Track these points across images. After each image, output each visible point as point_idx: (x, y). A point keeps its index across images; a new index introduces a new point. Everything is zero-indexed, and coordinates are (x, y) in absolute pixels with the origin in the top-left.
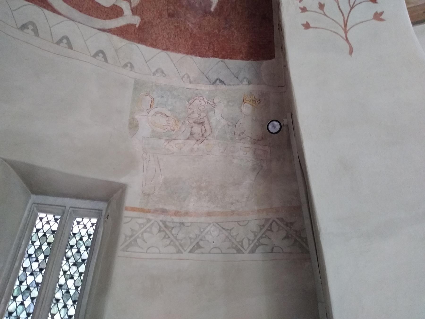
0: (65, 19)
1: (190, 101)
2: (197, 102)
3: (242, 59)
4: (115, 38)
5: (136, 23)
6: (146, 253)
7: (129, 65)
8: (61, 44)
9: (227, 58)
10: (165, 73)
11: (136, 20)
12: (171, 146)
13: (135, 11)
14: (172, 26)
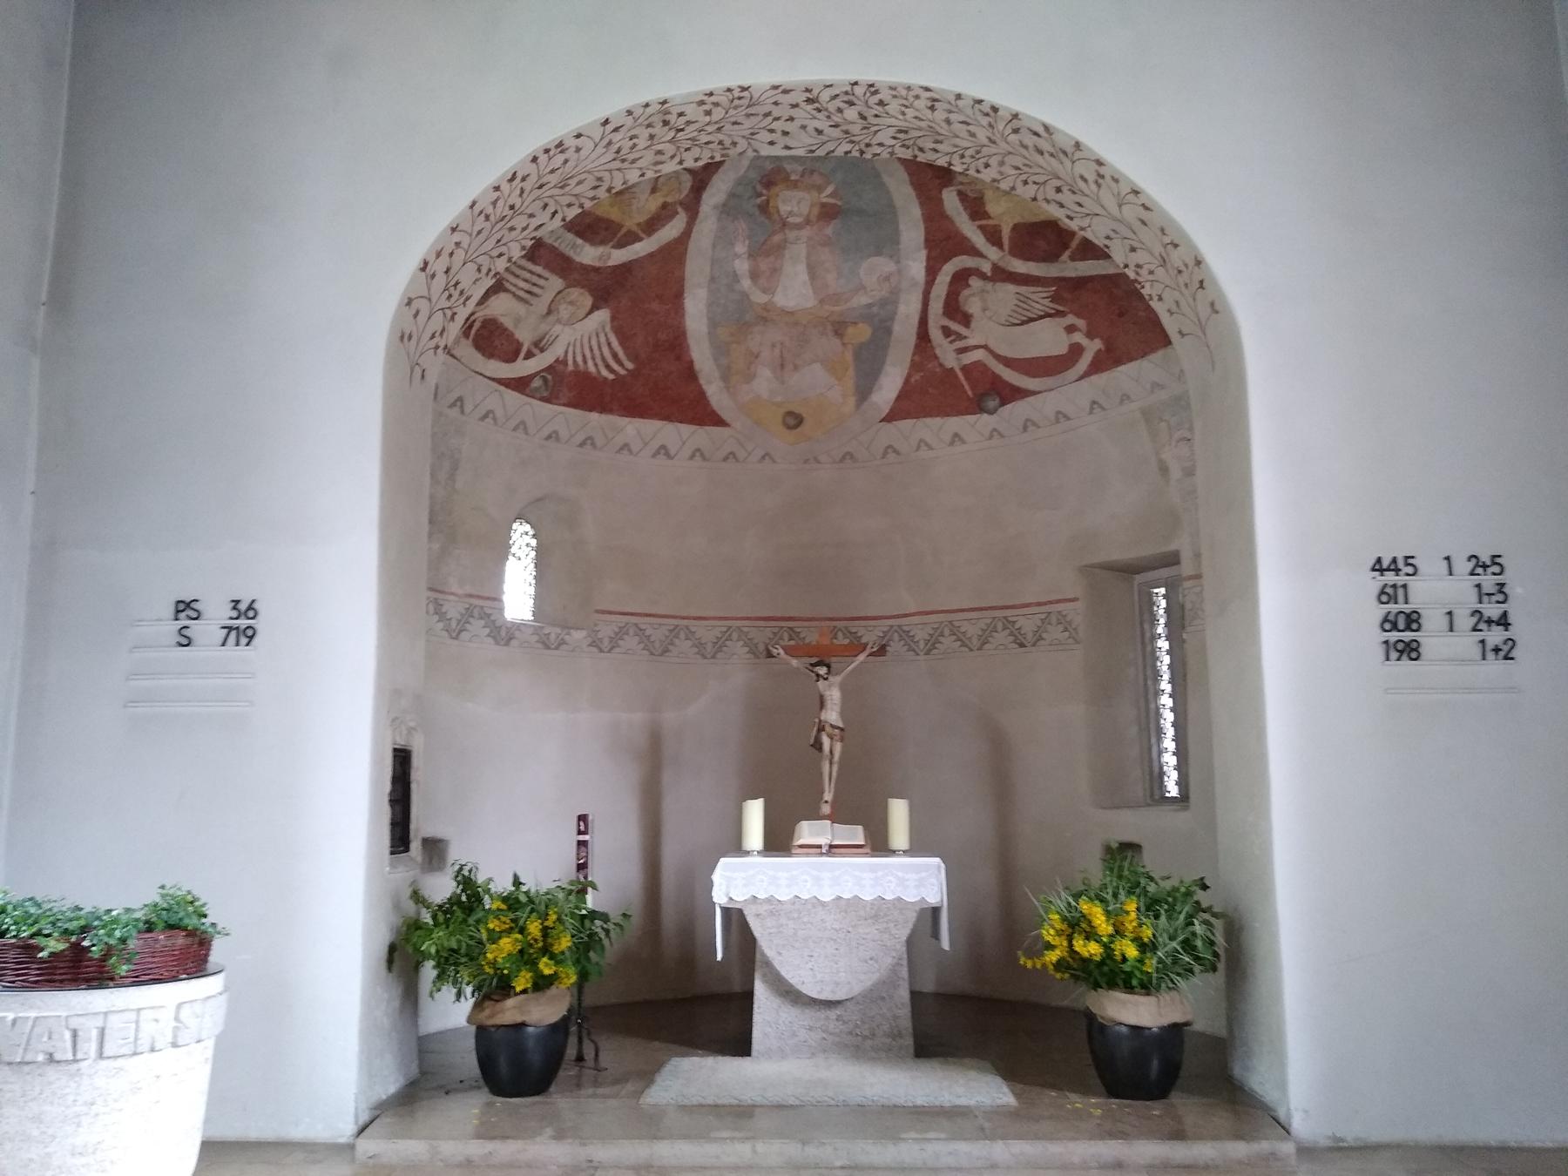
4: (1094, 378)
6: (750, 454)
8: (487, 420)
13: (1090, 335)
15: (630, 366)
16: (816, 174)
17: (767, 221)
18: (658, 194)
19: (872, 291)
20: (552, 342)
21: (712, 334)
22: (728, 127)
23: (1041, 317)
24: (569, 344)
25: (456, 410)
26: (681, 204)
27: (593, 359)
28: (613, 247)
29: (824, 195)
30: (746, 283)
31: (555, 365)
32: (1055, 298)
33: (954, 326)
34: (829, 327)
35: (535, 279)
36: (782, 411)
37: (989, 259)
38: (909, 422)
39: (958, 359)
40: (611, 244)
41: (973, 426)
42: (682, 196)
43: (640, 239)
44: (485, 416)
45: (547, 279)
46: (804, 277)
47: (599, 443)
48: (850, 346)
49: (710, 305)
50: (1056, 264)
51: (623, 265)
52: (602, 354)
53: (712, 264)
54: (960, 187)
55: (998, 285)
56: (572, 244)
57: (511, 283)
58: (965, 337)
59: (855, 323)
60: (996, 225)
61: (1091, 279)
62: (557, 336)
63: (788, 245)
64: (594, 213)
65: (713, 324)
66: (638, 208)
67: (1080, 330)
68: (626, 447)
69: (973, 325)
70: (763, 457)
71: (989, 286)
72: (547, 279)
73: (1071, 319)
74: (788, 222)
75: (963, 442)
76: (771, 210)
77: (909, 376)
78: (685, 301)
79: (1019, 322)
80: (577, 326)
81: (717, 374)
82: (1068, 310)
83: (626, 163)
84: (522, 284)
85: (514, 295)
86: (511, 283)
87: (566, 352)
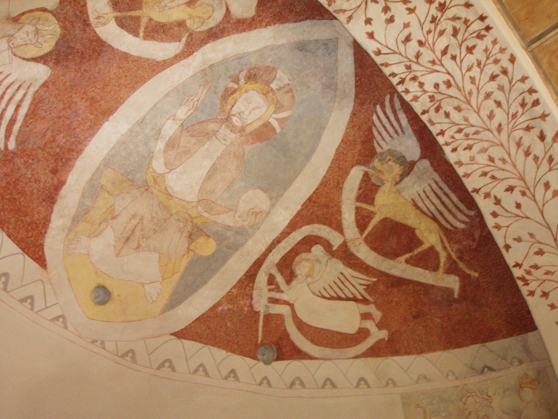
0: (322, 361)
1: (464, 400)
2: (470, 399)
3: (504, 337)
5: (384, 337)
6: (47, 308)
7: (390, 382)
9: (486, 342)
10: (428, 377)
11: (384, 334)
12: (212, 8)
13: (380, 326)
14: (420, 327)
16: (290, 95)
18: (188, 9)
21: (98, 172)
23: (348, 299)
26: (191, 35)
28: (116, 18)
29: (275, 116)
30: (161, 145)
33: (280, 279)
34: (189, 228)
37: (344, 236)
38: (197, 345)
39: (267, 307)
40: (119, 14)
42: (198, 30)
43: (136, 35)
46: (203, 172)
48: (191, 253)
49: (121, 143)
50: (392, 262)
53: (152, 109)
54: (370, 171)
55: (335, 260)
58: (282, 292)
60: (373, 212)
61: (410, 282)
63: (214, 137)
65: (107, 163)
69: (294, 283)
70: (57, 318)
73: (371, 309)
74: (231, 119)
75: (237, 379)
76: (231, 100)
77: (219, 304)
78: (106, 123)
79: (328, 296)
80: (17, 62)
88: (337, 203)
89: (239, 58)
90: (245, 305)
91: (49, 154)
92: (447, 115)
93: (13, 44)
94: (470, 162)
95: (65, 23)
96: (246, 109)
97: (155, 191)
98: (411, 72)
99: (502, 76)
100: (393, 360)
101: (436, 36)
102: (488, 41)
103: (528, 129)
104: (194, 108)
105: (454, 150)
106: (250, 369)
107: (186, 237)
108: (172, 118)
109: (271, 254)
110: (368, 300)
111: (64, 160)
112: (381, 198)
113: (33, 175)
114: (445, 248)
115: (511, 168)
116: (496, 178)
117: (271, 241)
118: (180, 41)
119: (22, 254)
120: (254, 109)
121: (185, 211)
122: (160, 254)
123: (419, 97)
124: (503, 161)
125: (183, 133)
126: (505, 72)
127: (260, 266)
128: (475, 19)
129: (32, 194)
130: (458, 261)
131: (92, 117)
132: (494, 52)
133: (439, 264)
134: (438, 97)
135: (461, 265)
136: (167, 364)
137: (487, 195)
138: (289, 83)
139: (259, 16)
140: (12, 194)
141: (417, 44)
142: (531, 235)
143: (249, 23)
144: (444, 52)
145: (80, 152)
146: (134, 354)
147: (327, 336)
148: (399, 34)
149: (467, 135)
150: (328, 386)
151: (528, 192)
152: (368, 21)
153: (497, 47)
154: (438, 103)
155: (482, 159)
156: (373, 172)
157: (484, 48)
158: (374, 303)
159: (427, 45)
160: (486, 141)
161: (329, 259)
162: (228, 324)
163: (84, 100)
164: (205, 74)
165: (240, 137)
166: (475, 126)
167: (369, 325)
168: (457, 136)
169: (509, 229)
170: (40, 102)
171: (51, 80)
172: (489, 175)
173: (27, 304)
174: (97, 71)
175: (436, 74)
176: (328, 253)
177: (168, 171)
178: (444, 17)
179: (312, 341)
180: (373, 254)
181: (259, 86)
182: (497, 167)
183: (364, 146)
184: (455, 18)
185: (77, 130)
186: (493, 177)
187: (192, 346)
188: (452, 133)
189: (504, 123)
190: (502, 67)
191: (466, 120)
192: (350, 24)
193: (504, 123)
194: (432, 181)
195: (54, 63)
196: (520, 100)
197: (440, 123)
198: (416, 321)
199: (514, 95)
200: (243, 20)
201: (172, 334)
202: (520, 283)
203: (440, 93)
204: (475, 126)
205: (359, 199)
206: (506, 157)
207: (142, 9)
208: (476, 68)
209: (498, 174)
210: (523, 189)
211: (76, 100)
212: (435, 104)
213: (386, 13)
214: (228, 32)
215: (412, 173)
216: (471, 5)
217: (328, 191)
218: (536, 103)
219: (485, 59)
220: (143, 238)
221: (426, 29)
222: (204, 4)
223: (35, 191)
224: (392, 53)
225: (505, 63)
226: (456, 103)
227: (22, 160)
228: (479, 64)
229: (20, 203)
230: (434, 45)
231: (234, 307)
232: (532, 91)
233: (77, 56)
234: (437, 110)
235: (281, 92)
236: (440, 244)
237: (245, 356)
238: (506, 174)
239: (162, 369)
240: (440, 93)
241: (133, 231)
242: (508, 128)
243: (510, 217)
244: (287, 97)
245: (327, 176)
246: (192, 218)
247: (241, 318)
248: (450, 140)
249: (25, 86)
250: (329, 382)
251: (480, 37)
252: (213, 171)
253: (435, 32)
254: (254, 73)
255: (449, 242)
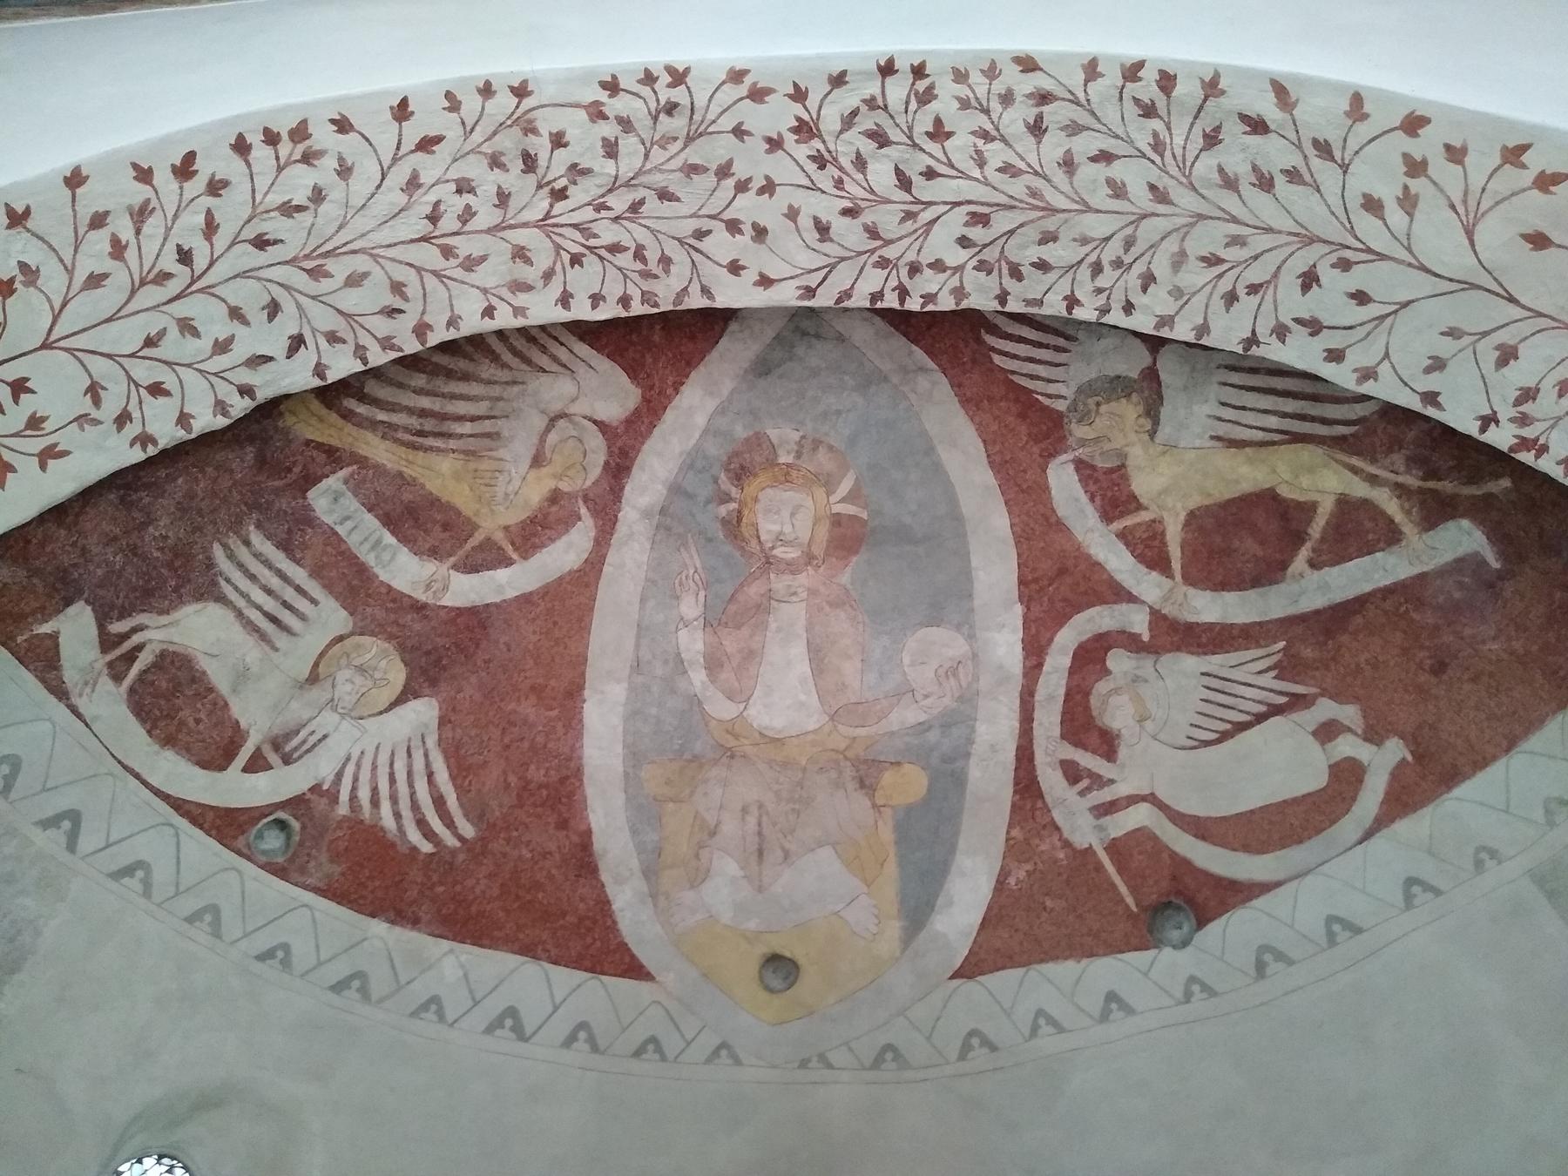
6: (689, 1044)
7: (1484, 855)
11: (1395, 751)
13: (1373, 735)
15: (468, 831)
16: (822, 450)
17: (737, 554)
18: (544, 470)
19: (926, 696)
20: (314, 745)
21: (631, 780)
22: (653, 205)
23: (1260, 718)
24: (348, 759)
25: (58, 836)
26: (586, 499)
27: (394, 799)
28: (455, 567)
29: (833, 499)
30: (698, 677)
31: (309, 796)
32: (1284, 669)
33: (1087, 760)
34: (849, 772)
35: (289, 594)
36: (762, 950)
37: (1143, 602)
38: (1011, 975)
39: (1101, 828)
40: (452, 560)
41: (1146, 974)
42: (588, 483)
43: (509, 563)
44: (128, 871)
45: (314, 602)
46: (803, 668)
47: (377, 988)
48: (888, 812)
50: (1282, 587)
51: (473, 611)
52: (413, 794)
53: (638, 637)
55: (1167, 659)
56: (373, 539)
57: (236, 588)
58: (1112, 781)
59: (898, 764)
60: (1154, 521)
61: (1359, 603)
62: (325, 737)
64: (423, 486)
65: (635, 757)
66: (507, 495)
67: (1349, 730)
68: (434, 1004)
69: (1123, 753)
70: (716, 1053)
71: (1147, 664)
72: (314, 602)
73: (1326, 709)
74: (775, 557)
75: (1129, 1010)
76: (746, 531)
79: (1214, 736)
81: (635, 863)
82: (1313, 690)
83: (453, 262)
84: (259, 596)
85: (240, 614)
86: (236, 588)
87: (339, 776)
88: (1077, 554)
89: (691, 466)
90: (1054, 848)
91: (535, 805)
92: (1042, 266)
93: (343, 708)
94: (1181, 302)
95: (386, 630)
96: (782, 524)
97: (749, 750)
98: (896, 265)
99: (1046, 109)
100: (1457, 799)
101: (859, 177)
102: (947, 91)
103: (1212, 139)
104: (701, 586)
105: (1129, 308)
106: (1146, 974)
107: (856, 790)
108: (681, 625)
109: (1035, 724)
110: (1304, 696)
111: (564, 800)
112: (1143, 484)
113: (531, 851)
114: (1373, 480)
115: (1265, 241)
116: (1261, 285)
117: (1018, 702)
118: (580, 519)
119: (593, 978)
120: (793, 515)
121: (820, 749)
122: (834, 845)
123: (962, 287)
124: (1236, 241)
125: (719, 634)
126: (1044, 98)
127: (1031, 759)
128: (879, 84)
129: (551, 877)
130: (1431, 484)
131: (554, 713)
132: (981, 91)
133: (1392, 521)
134: (991, 255)
135: (1447, 486)
136: (975, 1041)
137: (1281, 332)
138: (801, 434)
139: (652, 387)
140: (518, 897)
141: (847, 220)
142: (1452, 333)
143: (648, 410)
144: (904, 183)
145: (578, 772)
146: (896, 1049)
147: (1271, 822)
148: (800, 235)
149: (1118, 264)
150: (1342, 935)
151: (1348, 254)
152: (735, 268)
153: (976, 78)
154: (1003, 263)
155: (1195, 276)
156: (1087, 450)
157: (956, 105)
158: (1323, 695)
159: (863, 204)
160: (1162, 239)
161: (1155, 662)
162: (1049, 903)
163: (523, 699)
164: (668, 529)
165: (816, 571)
166: (1112, 235)
167: (1348, 747)
168: (1103, 281)
169: (1394, 358)
170: (458, 748)
171: (447, 710)
172: (1241, 292)
173: (650, 1054)
174: (505, 650)
175: (936, 227)
176: (1143, 654)
177: (742, 706)
178: (829, 139)
179: (1247, 848)
180: (1231, 597)
181: (763, 479)
182: (1239, 264)
183: (1028, 420)
184: (849, 120)
185: (549, 746)
186: (1253, 289)
187: (1003, 981)
188: (1090, 287)
189: (1154, 175)
190: (1030, 96)
191: (1084, 241)
192: (717, 298)
193: (1154, 175)
194: (1222, 370)
195: (429, 687)
196: (1131, 110)
197: (1049, 289)
198: (1445, 677)
199: (1111, 114)
200: (634, 413)
201: (952, 978)
202: (1526, 457)
203: (985, 246)
204: (1112, 235)
205: (1107, 517)
206: (1234, 229)
207: (479, 527)
208: (989, 146)
209: (1255, 275)
210: (1333, 258)
211: (510, 707)
212: (1000, 270)
213: (740, 232)
214: (633, 447)
215: (1164, 391)
216: (843, 73)
217: (1042, 544)
218: (1167, 81)
219: (984, 117)
220: (785, 837)
221: (827, 185)
222: (556, 446)
223: (554, 871)
224: (830, 271)
225: (1026, 85)
226: (1032, 233)
227: (501, 842)
228: (986, 136)
229: (541, 903)
230: (872, 192)
231: (1035, 864)
232: (1132, 72)
233: (453, 653)
234: (1016, 273)
235: (805, 457)
236: (1356, 479)
237: (1122, 952)
238: (1270, 262)
239: (970, 1055)
240: (985, 246)
241: (760, 834)
242: (1172, 177)
243: (1368, 334)
244: (822, 455)
245: (1017, 520)
246: (842, 753)
247: (1065, 876)
248: (1101, 300)
249: (416, 743)
250: (1338, 927)
251: (926, 97)
252: (816, 654)
253: (848, 175)
254: (738, 466)
255: (1374, 461)
